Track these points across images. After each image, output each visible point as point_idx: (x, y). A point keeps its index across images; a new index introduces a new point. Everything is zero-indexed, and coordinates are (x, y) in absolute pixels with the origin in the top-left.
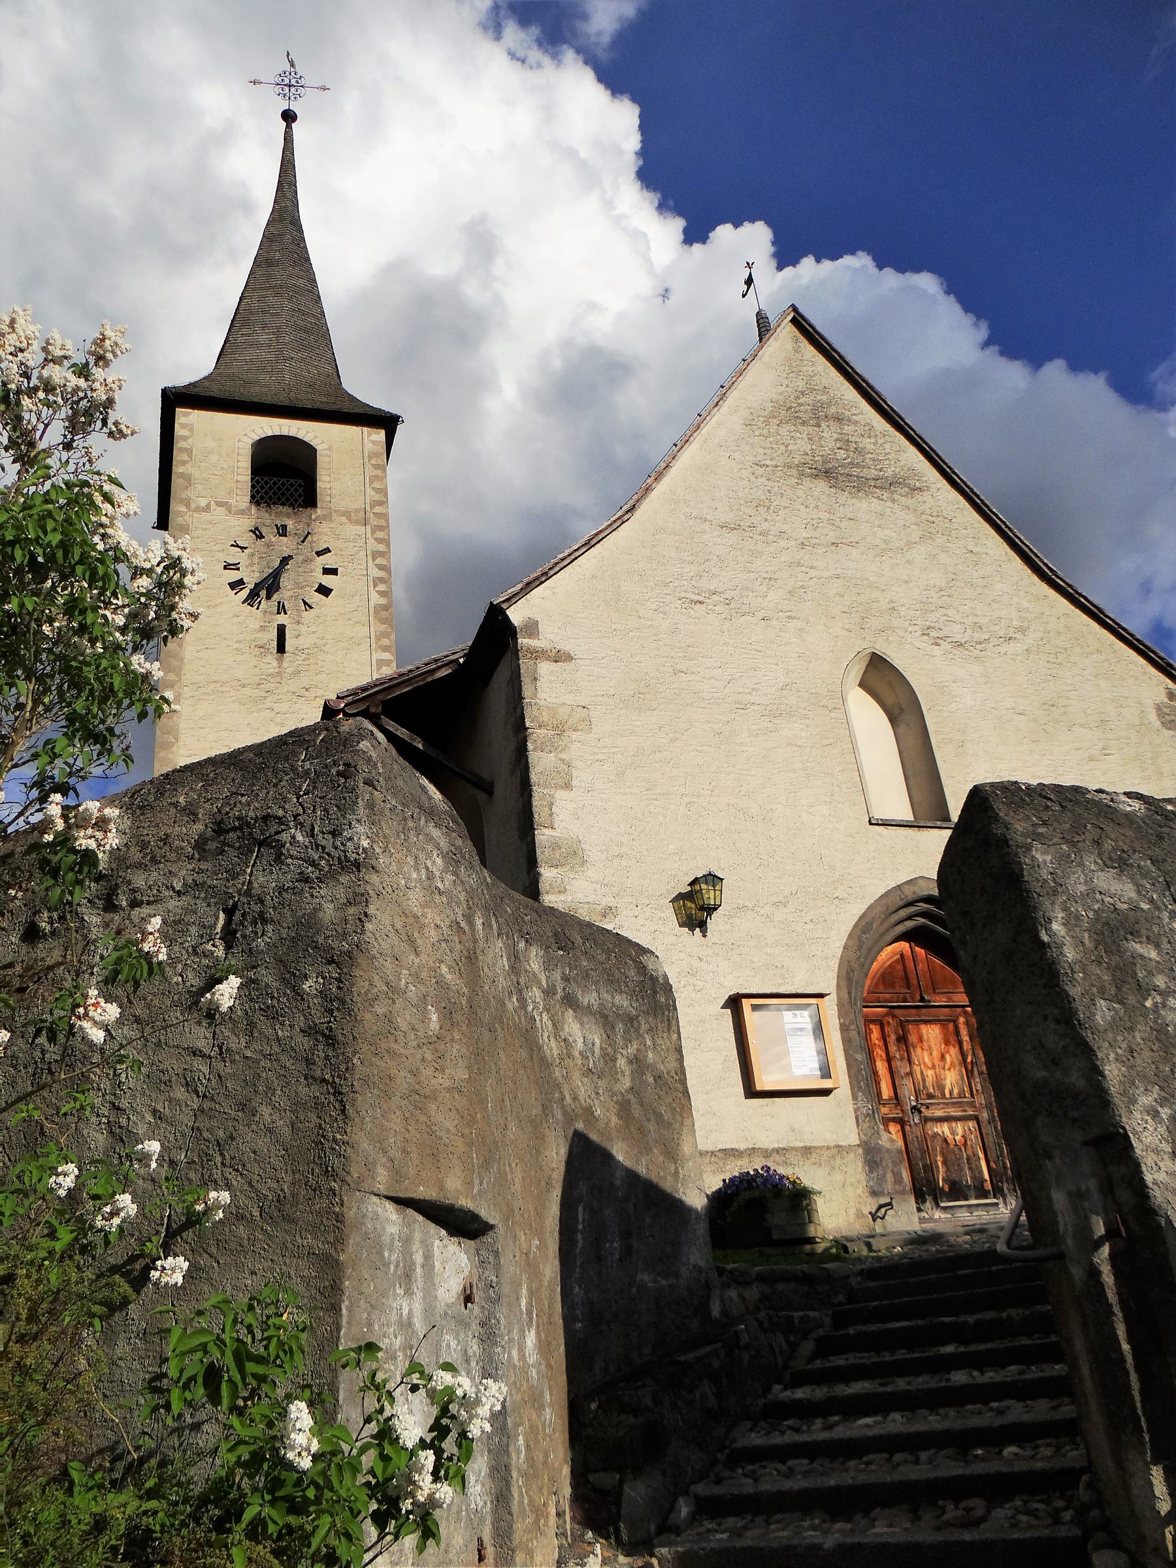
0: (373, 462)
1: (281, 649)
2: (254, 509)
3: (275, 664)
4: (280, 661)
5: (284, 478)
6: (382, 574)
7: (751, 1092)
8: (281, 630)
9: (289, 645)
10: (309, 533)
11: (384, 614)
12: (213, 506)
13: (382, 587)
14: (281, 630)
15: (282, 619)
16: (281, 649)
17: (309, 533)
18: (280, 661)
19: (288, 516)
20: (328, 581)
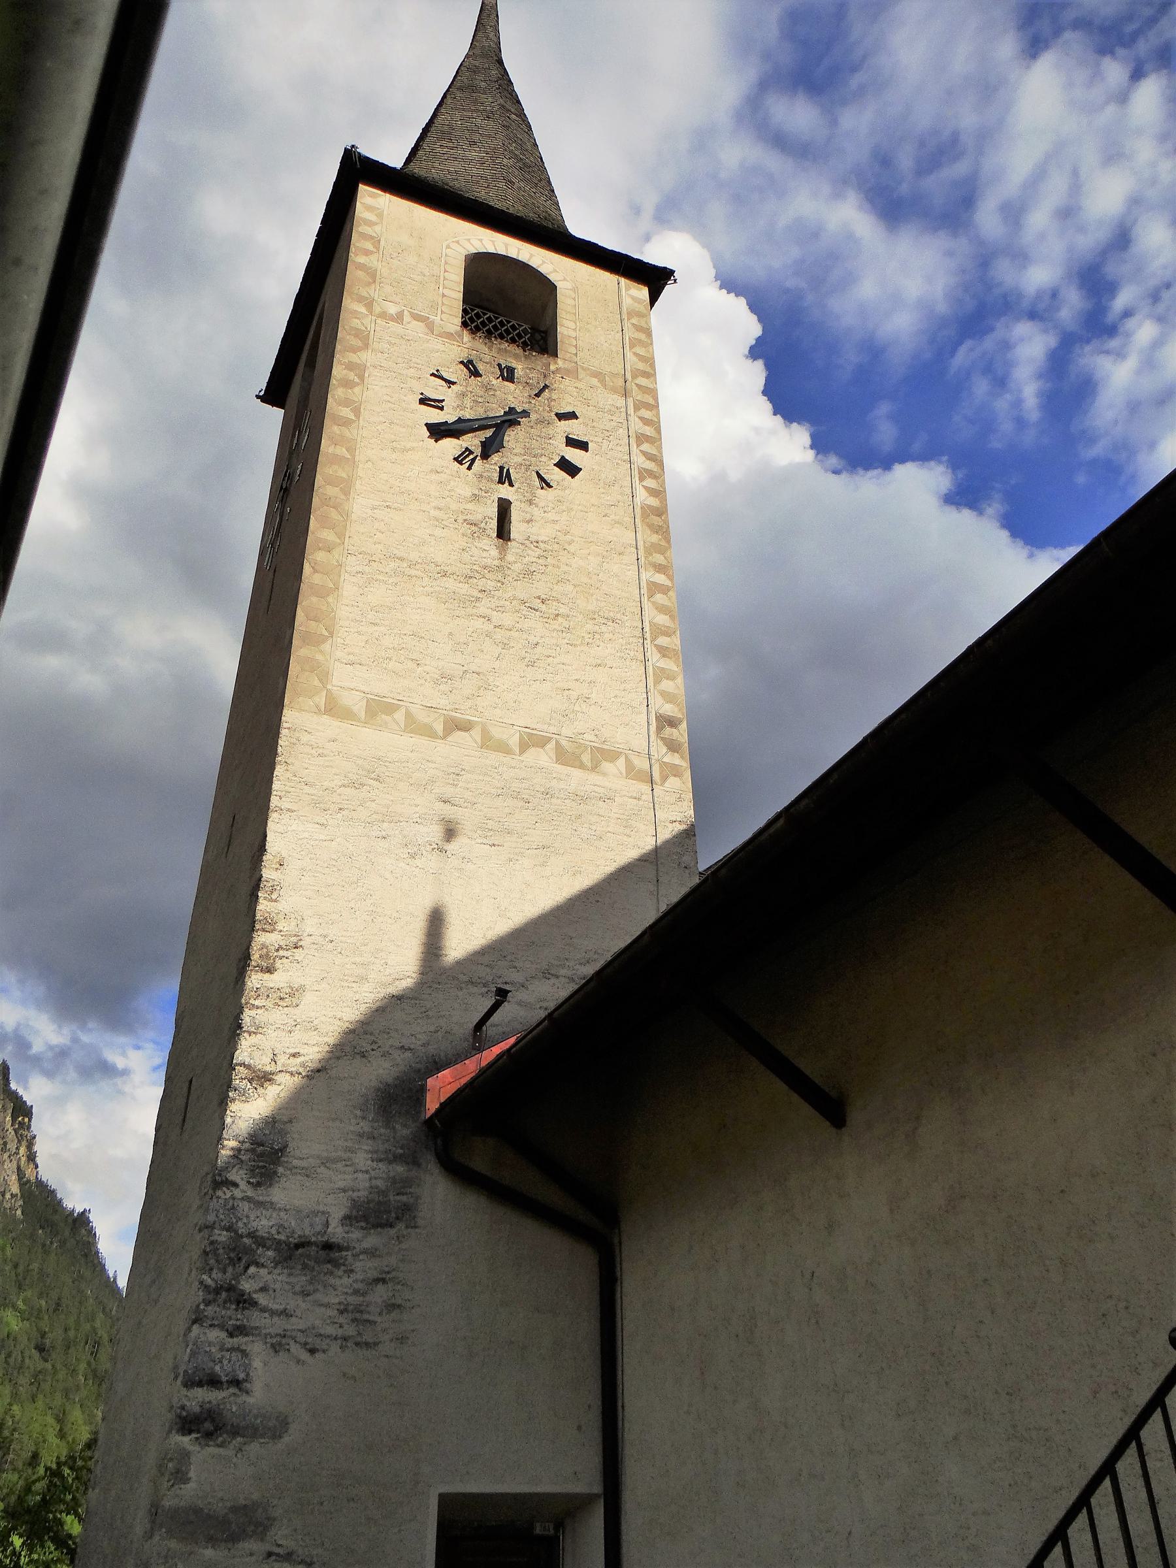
0: (634, 321)
1: (503, 532)
2: (466, 336)
3: (494, 552)
4: (503, 551)
5: (509, 311)
6: (650, 465)
7: (357, 171)
8: (504, 508)
9: (517, 528)
10: (546, 387)
11: (656, 520)
12: (407, 317)
13: (651, 483)
14: (504, 508)
15: (505, 491)
16: (503, 532)
17: (546, 387)
18: (503, 551)
19: (516, 357)
20: (574, 455)
